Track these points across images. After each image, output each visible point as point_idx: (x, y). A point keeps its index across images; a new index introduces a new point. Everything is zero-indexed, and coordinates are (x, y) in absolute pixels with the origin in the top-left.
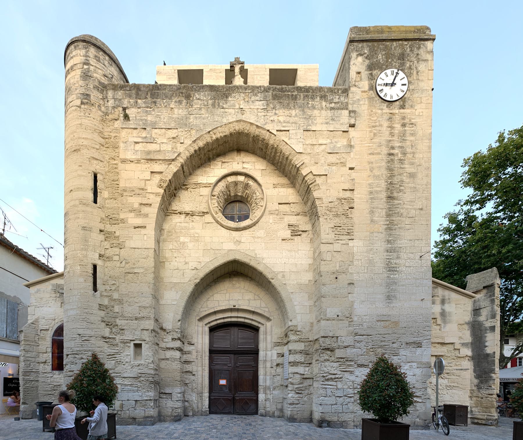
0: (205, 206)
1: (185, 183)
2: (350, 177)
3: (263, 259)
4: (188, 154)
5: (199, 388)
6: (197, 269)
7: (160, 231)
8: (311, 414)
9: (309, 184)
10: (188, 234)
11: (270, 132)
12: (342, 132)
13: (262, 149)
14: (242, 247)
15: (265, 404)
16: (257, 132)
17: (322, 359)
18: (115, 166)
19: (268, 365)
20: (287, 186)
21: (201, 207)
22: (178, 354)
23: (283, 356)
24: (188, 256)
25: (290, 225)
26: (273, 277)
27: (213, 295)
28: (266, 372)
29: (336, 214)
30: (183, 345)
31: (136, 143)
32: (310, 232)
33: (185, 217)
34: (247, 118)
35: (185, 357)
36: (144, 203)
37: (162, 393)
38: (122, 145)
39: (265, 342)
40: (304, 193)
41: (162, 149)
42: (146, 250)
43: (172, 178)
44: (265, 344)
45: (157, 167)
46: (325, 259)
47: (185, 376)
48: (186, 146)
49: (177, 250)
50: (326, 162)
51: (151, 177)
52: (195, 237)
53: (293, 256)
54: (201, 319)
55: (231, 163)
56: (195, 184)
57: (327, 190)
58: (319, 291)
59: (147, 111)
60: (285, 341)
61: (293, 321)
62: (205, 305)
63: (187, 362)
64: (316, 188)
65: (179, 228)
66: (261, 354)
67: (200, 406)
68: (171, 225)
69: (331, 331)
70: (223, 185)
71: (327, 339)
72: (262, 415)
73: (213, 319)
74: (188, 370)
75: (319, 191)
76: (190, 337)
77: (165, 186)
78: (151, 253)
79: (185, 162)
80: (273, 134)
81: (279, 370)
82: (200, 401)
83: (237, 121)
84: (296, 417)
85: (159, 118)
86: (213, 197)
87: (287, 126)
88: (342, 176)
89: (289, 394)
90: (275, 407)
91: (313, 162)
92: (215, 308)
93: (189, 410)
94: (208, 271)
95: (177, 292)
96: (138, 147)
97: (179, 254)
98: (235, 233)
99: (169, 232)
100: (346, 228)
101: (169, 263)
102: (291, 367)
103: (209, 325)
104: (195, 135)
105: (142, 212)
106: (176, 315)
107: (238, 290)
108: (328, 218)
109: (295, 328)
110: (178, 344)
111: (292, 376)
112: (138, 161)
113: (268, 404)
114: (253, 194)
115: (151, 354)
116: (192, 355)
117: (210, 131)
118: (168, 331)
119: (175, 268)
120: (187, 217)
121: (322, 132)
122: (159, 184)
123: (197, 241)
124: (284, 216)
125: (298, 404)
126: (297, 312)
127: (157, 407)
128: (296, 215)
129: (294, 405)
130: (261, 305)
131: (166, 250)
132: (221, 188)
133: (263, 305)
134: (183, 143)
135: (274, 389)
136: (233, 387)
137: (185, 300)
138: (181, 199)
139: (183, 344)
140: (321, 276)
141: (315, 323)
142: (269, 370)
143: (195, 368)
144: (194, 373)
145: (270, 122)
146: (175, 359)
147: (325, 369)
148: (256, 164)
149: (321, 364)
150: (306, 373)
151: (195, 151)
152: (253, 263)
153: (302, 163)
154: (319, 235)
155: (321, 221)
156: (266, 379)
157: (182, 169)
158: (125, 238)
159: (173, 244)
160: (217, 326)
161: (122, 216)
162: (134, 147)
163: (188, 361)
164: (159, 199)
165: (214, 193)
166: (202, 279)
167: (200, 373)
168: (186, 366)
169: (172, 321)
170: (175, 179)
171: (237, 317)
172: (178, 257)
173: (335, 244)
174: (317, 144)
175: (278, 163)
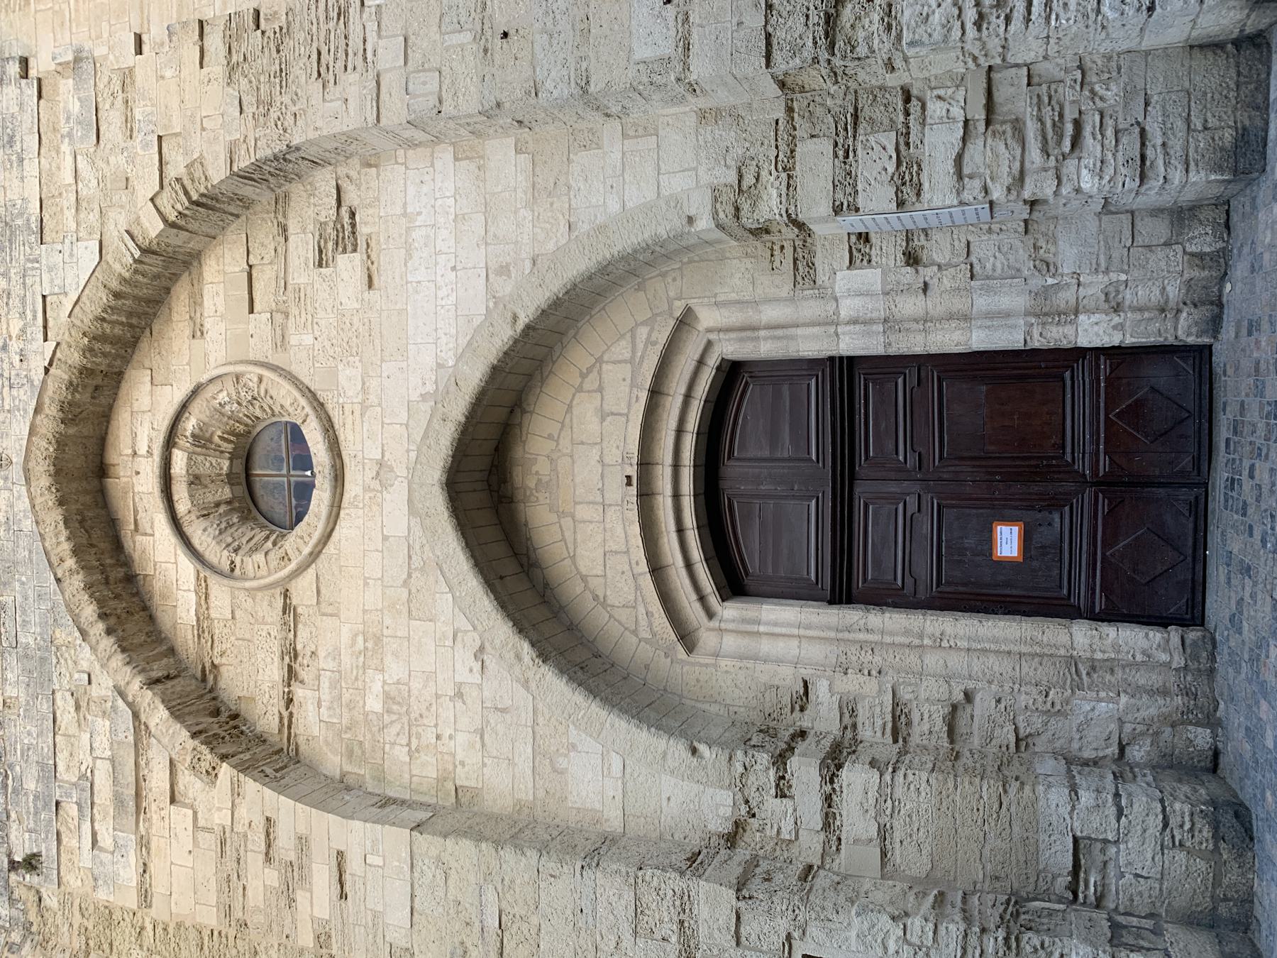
1: (199, 675)
2: (162, 44)
3: (439, 366)
4: (118, 660)
5: (1045, 673)
6: (482, 649)
7: (348, 789)
8: (1212, 46)
9: (187, 204)
10: (357, 679)
11: (51, 364)
12: (42, 102)
13: (97, 388)
14: (400, 456)
15: (1140, 310)
16: (51, 410)
17: (882, 44)
18: (159, 930)
19: (911, 305)
20: (195, 282)
21: (270, 620)
22: (856, 778)
23: (864, 238)
24: (432, 684)
25: (321, 259)
26: (509, 316)
27: (584, 578)
28: (950, 317)
29: (277, 80)
30: (811, 739)
32: (342, 171)
33: (302, 682)
34: (18, 447)
35: (873, 731)
36: (263, 847)
37: (1073, 888)
38: (102, 895)
39: (792, 331)
40: (215, 216)
41: (108, 753)
42: (419, 864)
43: (188, 728)
44: (799, 331)
45: (158, 780)
46: (433, 100)
47: (976, 742)
48: (98, 667)
49: (414, 730)
50: (123, 145)
51: (185, 805)
52: (366, 648)
53: (428, 236)
54: (687, 638)
55: (137, 500)
56: (199, 636)
57: (203, 129)
58: (561, 108)
60: (791, 233)
61: (692, 212)
62: (623, 615)
63: (899, 726)
64: (198, 174)
65: (338, 711)
66: (850, 344)
67: (1155, 679)
68: (326, 741)
69: (740, 24)
70: (200, 532)
71: (779, 35)
72: (1215, 324)
74: (940, 726)
75: (209, 160)
77: (209, 757)
78: (428, 844)
79: (140, 672)
80: (54, 352)
81: (938, 250)
82: (1119, 674)
83: (28, 480)
84: (1228, 136)
85: (30, 753)
86: (237, 571)
87: (34, 300)
88: (163, 77)
89: (1078, 190)
90: (1160, 253)
91: (124, 197)
92: (638, 570)
93: (1180, 744)
95: (573, 747)
96: (106, 840)
97: (425, 721)
98: (352, 488)
99: (350, 753)
100: (323, 27)
101: (459, 767)
102: (926, 195)
103: (713, 600)
104: (66, 634)
105: (292, 856)
106: (670, 762)
107: (563, 463)
108: (294, 109)
109: (724, 198)
110: (805, 770)
111: (977, 184)
112: (144, 844)
113: (1147, 293)
114: (223, 415)
115: (856, 921)
116: (864, 698)
117: (55, 575)
118: (744, 809)
119: (478, 746)
120: (303, 674)
121: (43, 173)
122: (204, 776)
123: (378, 640)
124: (290, 287)
125: (1143, 132)
126: (651, 195)
127: (1157, 932)
129: (1150, 153)
130: (625, 361)
131: (412, 776)
132: (209, 540)
133: (622, 349)
134: (89, 675)
135: (1047, 266)
136: (1035, 488)
137: (605, 713)
138: (244, 693)
139: (803, 734)
140: (498, 105)
141: (702, 102)
142: (936, 304)
146: (882, 797)
147: (936, 18)
148: (136, 406)
149: (912, 44)
150: (957, 112)
151: (109, 632)
152: (458, 409)
153: (127, 238)
154: (350, 138)
156: (990, 315)
157: (160, 686)
158: (380, 940)
159: (393, 744)
160: (716, 562)
161: (306, 939)
162: (106, 851)
164: (251, 786)
165: (226, 566)
166: (521, 628)
167: (957, 662)
168: (918, 733)
169: (696, 788)
170: (190, 713)
171: (676, 466)
172: (436, 726)
173: (381, 66)
174: (74, 187)
175: (131, 326)
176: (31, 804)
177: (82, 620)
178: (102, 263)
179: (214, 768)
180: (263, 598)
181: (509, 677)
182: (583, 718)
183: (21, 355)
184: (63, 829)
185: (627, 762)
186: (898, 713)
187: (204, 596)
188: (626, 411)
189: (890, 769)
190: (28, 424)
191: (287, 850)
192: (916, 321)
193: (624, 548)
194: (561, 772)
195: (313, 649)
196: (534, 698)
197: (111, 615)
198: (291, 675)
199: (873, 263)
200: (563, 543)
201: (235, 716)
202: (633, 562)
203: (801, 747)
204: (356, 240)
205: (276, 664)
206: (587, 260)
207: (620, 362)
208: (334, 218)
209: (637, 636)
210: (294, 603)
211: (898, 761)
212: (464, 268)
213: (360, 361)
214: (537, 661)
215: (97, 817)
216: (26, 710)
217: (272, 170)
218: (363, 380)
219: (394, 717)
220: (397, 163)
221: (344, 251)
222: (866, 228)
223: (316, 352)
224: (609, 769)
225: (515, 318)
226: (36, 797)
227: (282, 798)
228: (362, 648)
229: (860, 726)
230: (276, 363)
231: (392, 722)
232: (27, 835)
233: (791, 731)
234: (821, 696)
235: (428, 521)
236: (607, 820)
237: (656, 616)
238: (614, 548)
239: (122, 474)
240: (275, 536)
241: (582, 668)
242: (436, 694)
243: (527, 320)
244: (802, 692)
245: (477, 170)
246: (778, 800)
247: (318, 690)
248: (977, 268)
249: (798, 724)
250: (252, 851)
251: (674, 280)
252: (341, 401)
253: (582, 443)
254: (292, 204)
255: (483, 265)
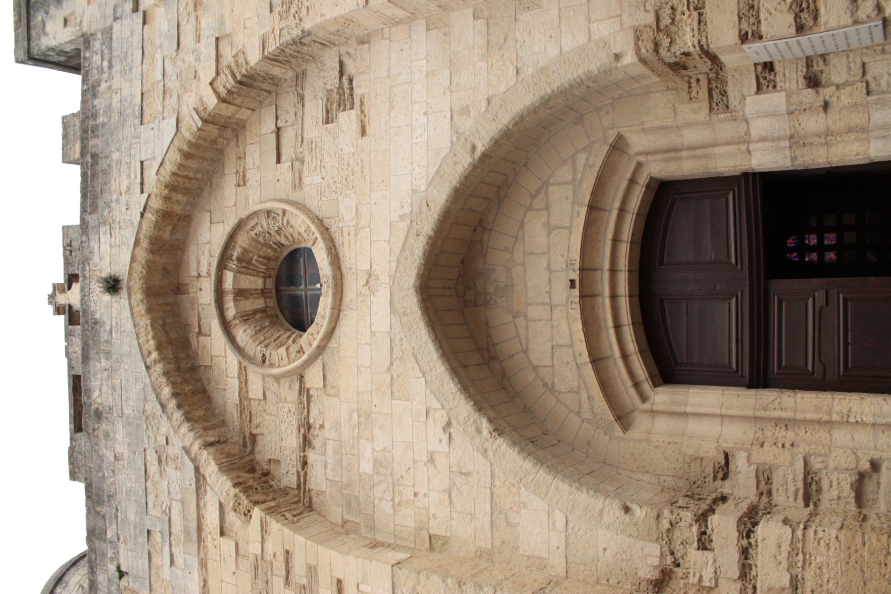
0: (287, 386)
3: (414, 191)
6: (449, 424)
10: (353, 447)
12: (146, 27)
14: (384, 268)
16: (145, 244)
19: (813, 123)
23: (769, 66)
25: (328, 117)
26: (469, 146)
27: (535, 368)
28: (850, 130)
30: (730, 503)
31: (172, 562)
32: (343, 50)
36: (284, 572)
40: (253, 93)
41: (179, 496)
43: (232, 479)
44: (717, 150)
48: (172, 432)
52: (359, 423)
55: (200, 310)
56: (241, 413)
57: (245, 28)
59: (122, 519)
60: (704, 66)
64: (241, 60)
65: (339, 472)
73: (623, 370)
74: (848, 493)
76: (695, 467)
86: (267, 361)
94: (452, 385)
95: (524, 505)
96: (179, 560)
99: (349, 506)
101: (432, 519)
102: (822, 18)
103: (647, 387)
105: (304, 581)
106: (606, 519)
109: (645, 36)
112: (203, 564)
116: (778, 467)
117: (145, 363)
118: (669, 560)
119: (447, 502)
122: (243, 517)
123: (368, 416)
124: (305, 141)
128: (303, 106)
130: (567, 183)
131: (395, 525)
132: (248, 338)
133: (564, 174)
139: (724, 499)
143: (844, 459)
144: (865, 466)
145: (129, 212)
146: (793, 551)
152: (427, 225)
153: (194, 113)
155: (313, 25)
163: (807, 485)
164: (275, 526)
166: (480, 408)
168: (828, 496)
172: (414, 485)
176: (132, 531)
177: (162, 397)
178: (178, 133)
179: (249, 511)
180: (285, 383)
181: (471, 448)
182: (532, 481)
183: (127, 205)
184: (152, 550)
185: (570, 519)
186: (809, 481)
187: (244, 383)
188: (569, 224)
189: (802, 526)
190: (130, 254)
191: (301, 576)
192: (819, 136)
193: (568, 342)
194: (514, 526)
195: (321, 422)
196: (491, 465)
197: (181, 394)
198: (306, 443)
199: (778, 88)
200: (517, 339)
201: (266, 474)
202: (577, 354)
203: (721, 508)
204: (353, 100)
205: (294, 434)
206: (531, 96)
207: (563, 183)
208: (337, 86)
209: (580, 417)
210: (307, 386)
211: (808, 521)
212: (433, 112)
213: (355, 193)
214: (494, 434)
215: (173, 543)
216: (128, 462)
217: (292, 52)
218: (356, 207)
219: (382, 478)
220: (383, 38)
221: (344, 110)
222: (770, 56)
223: (323, 188)
224: (554, 524)
225: (474, 148)
226: (135, 527)
227: (297, 536)
228: (357, 422)
229: (774, 492)
230: (295, 200)
231: (380, 482)
232: (130, 553)
233: (713, 496)
234: (740, 466)
235: (405, 319)
236: (552, 566)
237: (597, 399)
238: (560, 342)
239: (191, 291)
240: (294, 336)
241: (532, 442)
242: (414, 460)
243: (483, 149)
244: (723, 463)
245: (444, 36)
246: (700, 552)
247: (325, 455)
248: (873, 85)
249: (720, 490)
250: (276, 575)
251: (607, 113)
252: (340, 225)
253: (533, 254)
254: (308, 79)
255: (448, 108)
